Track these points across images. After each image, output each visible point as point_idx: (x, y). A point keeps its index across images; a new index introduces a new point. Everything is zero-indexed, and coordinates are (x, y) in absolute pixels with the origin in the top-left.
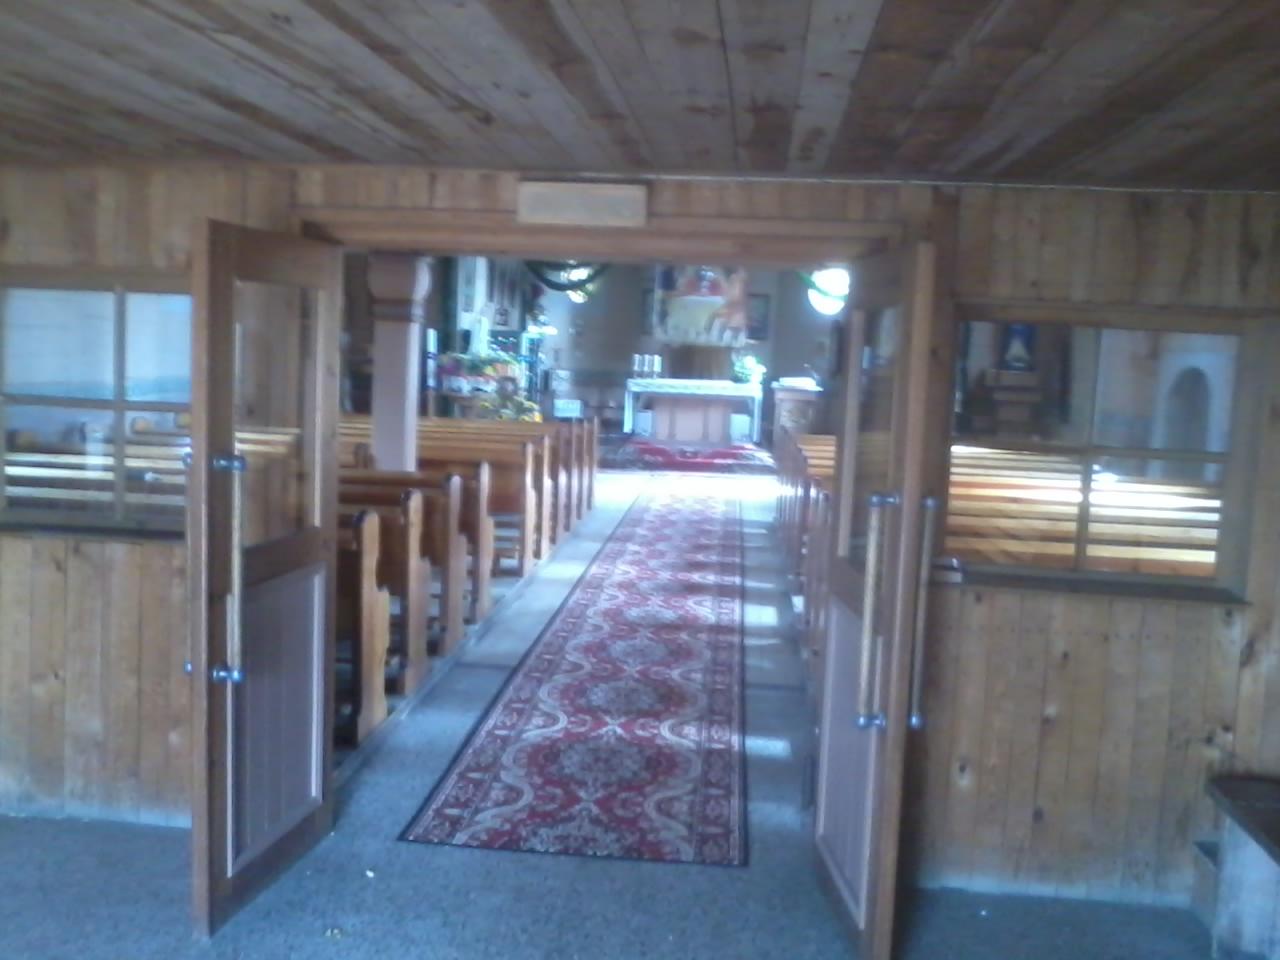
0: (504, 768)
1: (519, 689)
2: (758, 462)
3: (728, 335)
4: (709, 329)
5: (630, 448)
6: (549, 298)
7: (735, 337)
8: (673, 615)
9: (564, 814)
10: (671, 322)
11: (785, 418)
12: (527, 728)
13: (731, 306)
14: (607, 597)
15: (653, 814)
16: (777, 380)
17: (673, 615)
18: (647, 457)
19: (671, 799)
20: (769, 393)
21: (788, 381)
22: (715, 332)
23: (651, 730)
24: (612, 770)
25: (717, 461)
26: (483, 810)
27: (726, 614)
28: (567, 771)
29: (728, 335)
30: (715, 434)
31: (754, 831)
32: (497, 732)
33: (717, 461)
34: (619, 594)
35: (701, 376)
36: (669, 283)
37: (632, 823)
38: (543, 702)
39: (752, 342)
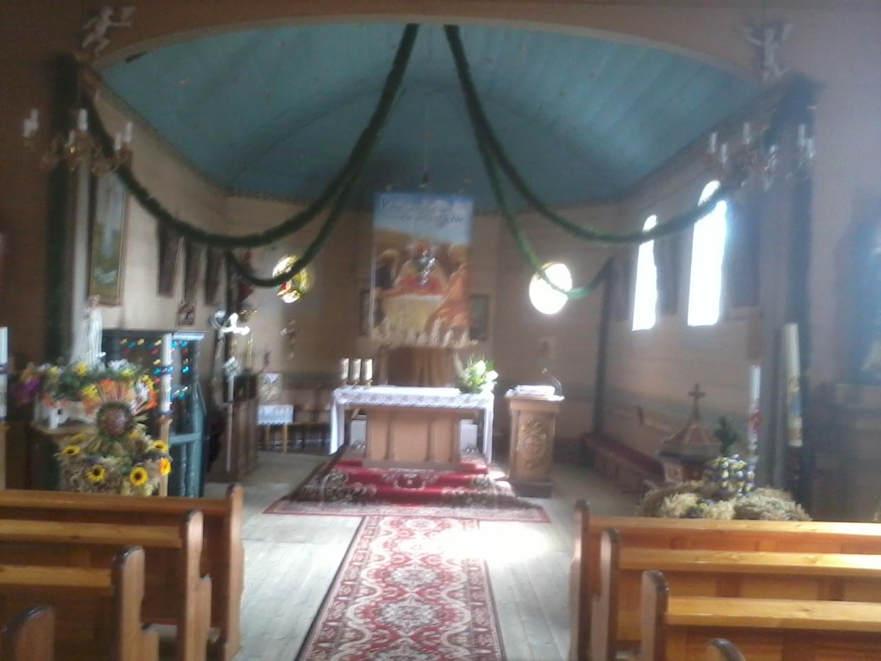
0: (363, 579)
1: (360, 544)
2: (496, 492)
3: (448, 335)
4: (428, 328)
5: (337, 473)
6: (258, 296)
7: (457, 336)
9: (393, 644)
10: (388, 322)
11: (523, 440)
12: (358, 595)
13: (450, 304)
14: (385, 533)
15: (446, 644)
18: (358, 487)
19: (455, 591)
20: (501, 405)
21: (524, 390)
22: (435, 333)
23: (435, 641)
24: (416, 618)
25: (445, 491)
26: (343, 643)
27: (475, 571)
28: (389, 620)
30: (440, 454)
31: (491, 575)
32: (355, 563)
33: (445, 491)
34: (392, 530)
36: (384, 281)
37: (436, 601)
38: (364, 580)
39: (475, 343)
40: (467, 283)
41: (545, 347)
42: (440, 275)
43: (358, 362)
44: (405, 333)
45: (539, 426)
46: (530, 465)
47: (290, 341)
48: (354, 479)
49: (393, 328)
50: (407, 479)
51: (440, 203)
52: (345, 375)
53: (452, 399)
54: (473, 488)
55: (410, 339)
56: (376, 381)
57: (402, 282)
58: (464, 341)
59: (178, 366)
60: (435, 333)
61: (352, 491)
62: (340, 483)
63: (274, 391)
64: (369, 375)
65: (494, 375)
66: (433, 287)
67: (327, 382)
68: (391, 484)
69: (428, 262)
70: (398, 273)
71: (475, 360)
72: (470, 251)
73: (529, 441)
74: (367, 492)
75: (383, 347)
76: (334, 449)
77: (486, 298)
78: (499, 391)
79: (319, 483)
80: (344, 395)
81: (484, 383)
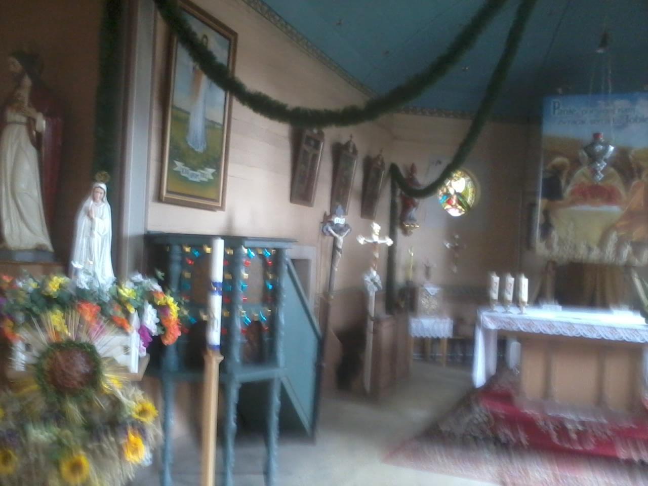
3: (626, 251)
4: (602, 243)
5: (480, 412)
8: (135, 407)
10: (555, 234)
13: (631, 215)
17: (135, 407)
22: (610, 248)
29: (626, 251)
36: (553, 191)
42: (617, 182)
44: (575, 248)
47: (454, 256)
51: (620, 104)
55: (582, 253)
56: (537, 299)
57: (573, 193)
59: (259, 280)
60: (610, 248)
63: (435, 304)
64: (524, 295)
66: (609, 196)
67: (481, 298)
69: (606, 150)
70: (568, 182)
75: (552, 264)
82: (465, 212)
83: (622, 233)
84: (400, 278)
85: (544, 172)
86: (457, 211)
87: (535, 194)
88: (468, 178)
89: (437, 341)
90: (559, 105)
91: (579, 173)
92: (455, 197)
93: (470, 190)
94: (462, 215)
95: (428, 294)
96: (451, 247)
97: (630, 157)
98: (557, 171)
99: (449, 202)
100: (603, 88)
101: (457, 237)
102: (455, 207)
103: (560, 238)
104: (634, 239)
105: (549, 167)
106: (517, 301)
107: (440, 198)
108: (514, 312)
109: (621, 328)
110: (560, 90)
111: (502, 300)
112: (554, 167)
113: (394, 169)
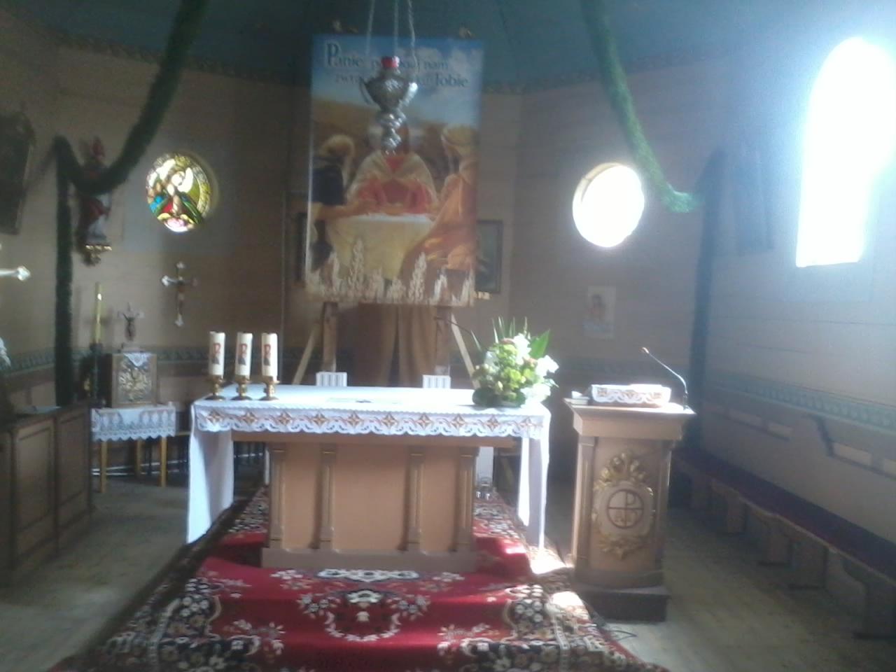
3: (441, 283)
4: (406, 273)
10: (335, 261)
13: (445, 230)
16: (585, 390)
21: (608, 393)
22: (418, 280)
35: (393, 380)
36: (330, 192)
40: (473, 199)
41: (599, 303)
42: (422, 177)
43: (248, 338)
44: (366, 283)
45: (639, 469)
46: (619, 552)
47: (176, 300)
48: (233, 609)
49: (345, 273)
50: (357, 608)
52: (219, 370)
53: (458, 419)
54: (507, 629)
55: (376, 289)
57: (360, 193)
58: (467, 290)
60: (418, 280)
61: (226, 646)
62: (200, 620)
65: (548, 364)
66: (415, 201)
68: (320, 622)
69: (405, 89)
70: (352, 176)
71: (507, 333)
72: (476, 139)
73: (618, 500)
74: (260, 652)
76: (198, 523)
77: (499, 223)
78: (556, 403)
79: (153, 623)
80: (215, 414)
81: (529, 383)
82: (195, 224)
83: (432, 257)
84: (82, 340)
85: (317, 158)
86: (181, 222)
87: (305, 197)
88: (198, 168)
89: (152, 443)
90: (337, 50)
91: (368, 160)
92: (176, 200)
93: (202, 189)
94: (190, 231)
95: (131, 366)
96: (172, 284)
97: (443, 138)
98: (336, 157)
99: (166, 208)
100: (493, 322)
101: (181, 266)
102: (178, 217)
103: (342, 266)
104: (449, 266)
105: (323, 152)
106: (258, 374)
107: (150, 201)
108: (255, 394)
109: (436, 415)
110: (337, 25)
111: (231, 376)
112: (331, 151)
113: (60, 148)
